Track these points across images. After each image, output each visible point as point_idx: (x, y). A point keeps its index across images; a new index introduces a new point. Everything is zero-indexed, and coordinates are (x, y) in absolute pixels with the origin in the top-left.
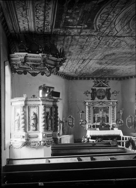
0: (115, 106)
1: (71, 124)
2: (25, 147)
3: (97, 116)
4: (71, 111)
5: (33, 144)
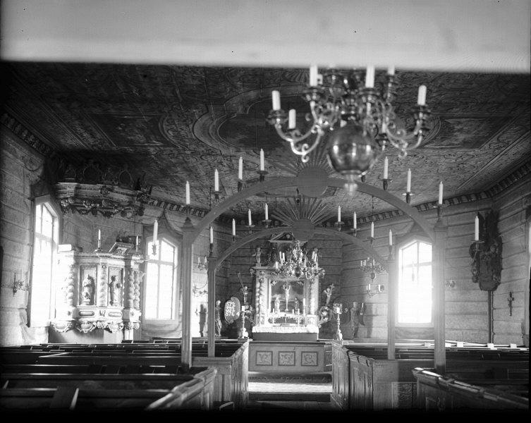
2: (71, 331)
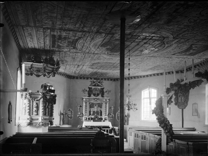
0: (107, 103)
1: (70, 116)
2: (29, 126)
3: (93, 110)
4: (72, 106)
5: (35, 124)
